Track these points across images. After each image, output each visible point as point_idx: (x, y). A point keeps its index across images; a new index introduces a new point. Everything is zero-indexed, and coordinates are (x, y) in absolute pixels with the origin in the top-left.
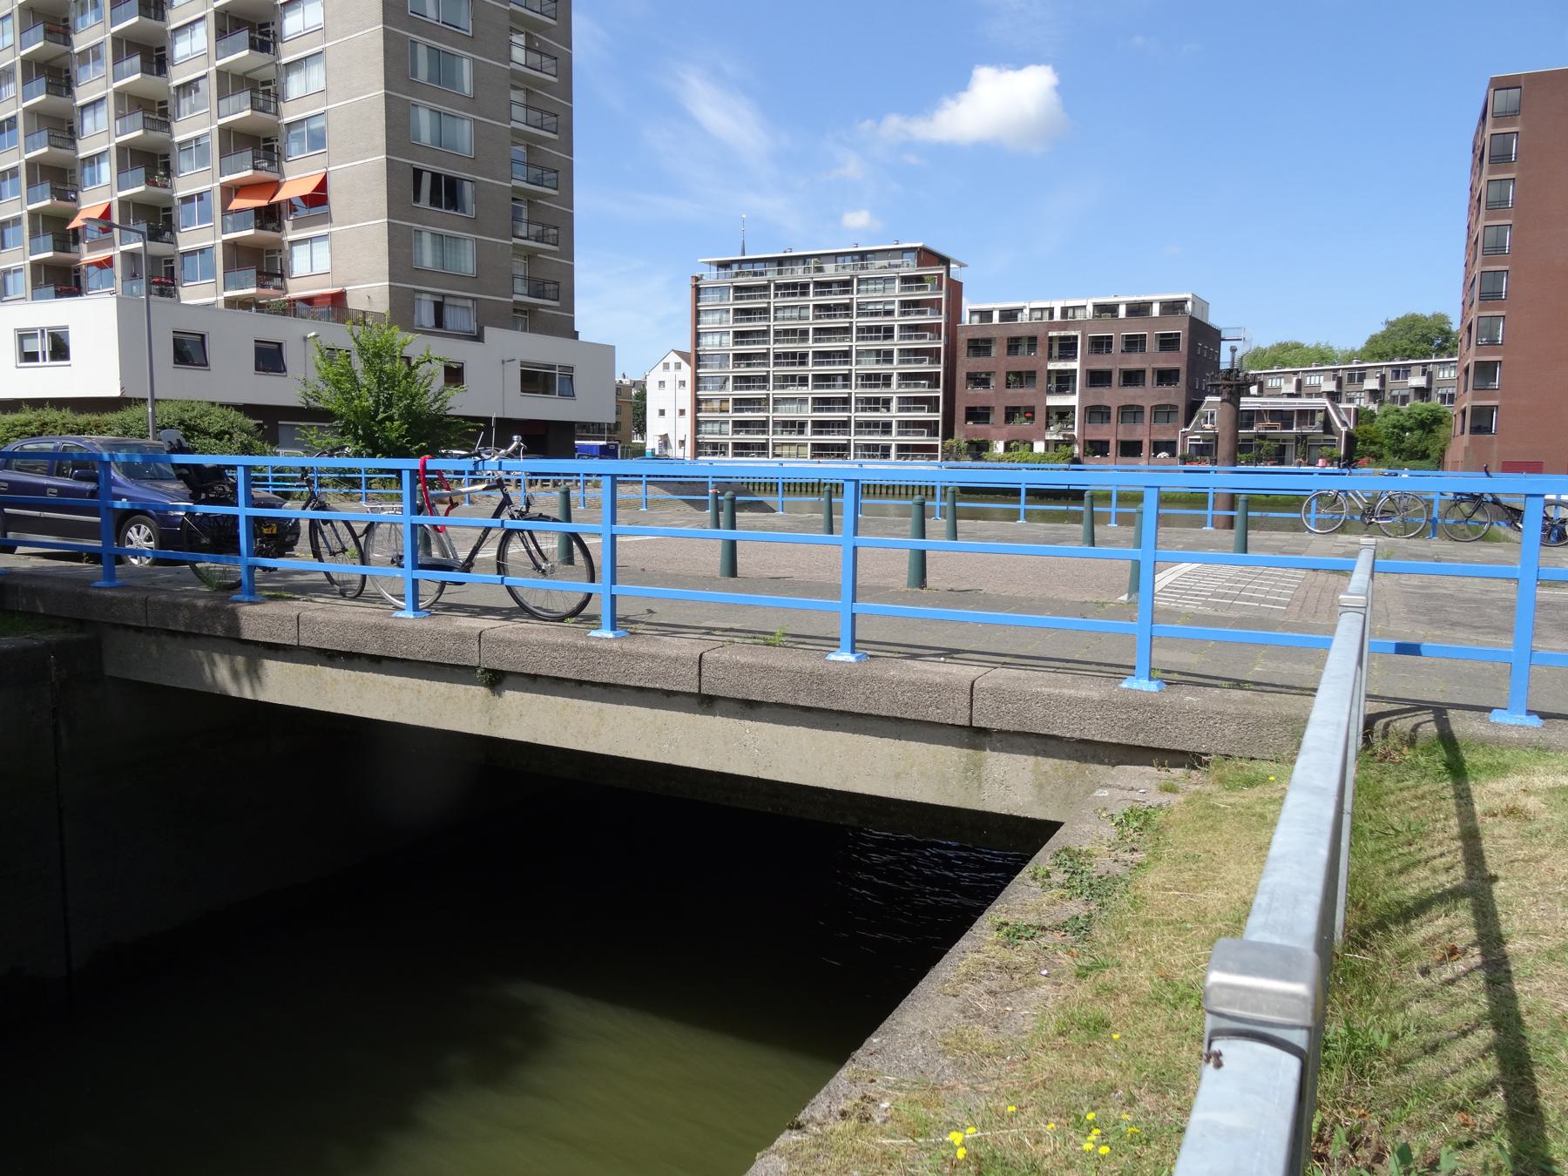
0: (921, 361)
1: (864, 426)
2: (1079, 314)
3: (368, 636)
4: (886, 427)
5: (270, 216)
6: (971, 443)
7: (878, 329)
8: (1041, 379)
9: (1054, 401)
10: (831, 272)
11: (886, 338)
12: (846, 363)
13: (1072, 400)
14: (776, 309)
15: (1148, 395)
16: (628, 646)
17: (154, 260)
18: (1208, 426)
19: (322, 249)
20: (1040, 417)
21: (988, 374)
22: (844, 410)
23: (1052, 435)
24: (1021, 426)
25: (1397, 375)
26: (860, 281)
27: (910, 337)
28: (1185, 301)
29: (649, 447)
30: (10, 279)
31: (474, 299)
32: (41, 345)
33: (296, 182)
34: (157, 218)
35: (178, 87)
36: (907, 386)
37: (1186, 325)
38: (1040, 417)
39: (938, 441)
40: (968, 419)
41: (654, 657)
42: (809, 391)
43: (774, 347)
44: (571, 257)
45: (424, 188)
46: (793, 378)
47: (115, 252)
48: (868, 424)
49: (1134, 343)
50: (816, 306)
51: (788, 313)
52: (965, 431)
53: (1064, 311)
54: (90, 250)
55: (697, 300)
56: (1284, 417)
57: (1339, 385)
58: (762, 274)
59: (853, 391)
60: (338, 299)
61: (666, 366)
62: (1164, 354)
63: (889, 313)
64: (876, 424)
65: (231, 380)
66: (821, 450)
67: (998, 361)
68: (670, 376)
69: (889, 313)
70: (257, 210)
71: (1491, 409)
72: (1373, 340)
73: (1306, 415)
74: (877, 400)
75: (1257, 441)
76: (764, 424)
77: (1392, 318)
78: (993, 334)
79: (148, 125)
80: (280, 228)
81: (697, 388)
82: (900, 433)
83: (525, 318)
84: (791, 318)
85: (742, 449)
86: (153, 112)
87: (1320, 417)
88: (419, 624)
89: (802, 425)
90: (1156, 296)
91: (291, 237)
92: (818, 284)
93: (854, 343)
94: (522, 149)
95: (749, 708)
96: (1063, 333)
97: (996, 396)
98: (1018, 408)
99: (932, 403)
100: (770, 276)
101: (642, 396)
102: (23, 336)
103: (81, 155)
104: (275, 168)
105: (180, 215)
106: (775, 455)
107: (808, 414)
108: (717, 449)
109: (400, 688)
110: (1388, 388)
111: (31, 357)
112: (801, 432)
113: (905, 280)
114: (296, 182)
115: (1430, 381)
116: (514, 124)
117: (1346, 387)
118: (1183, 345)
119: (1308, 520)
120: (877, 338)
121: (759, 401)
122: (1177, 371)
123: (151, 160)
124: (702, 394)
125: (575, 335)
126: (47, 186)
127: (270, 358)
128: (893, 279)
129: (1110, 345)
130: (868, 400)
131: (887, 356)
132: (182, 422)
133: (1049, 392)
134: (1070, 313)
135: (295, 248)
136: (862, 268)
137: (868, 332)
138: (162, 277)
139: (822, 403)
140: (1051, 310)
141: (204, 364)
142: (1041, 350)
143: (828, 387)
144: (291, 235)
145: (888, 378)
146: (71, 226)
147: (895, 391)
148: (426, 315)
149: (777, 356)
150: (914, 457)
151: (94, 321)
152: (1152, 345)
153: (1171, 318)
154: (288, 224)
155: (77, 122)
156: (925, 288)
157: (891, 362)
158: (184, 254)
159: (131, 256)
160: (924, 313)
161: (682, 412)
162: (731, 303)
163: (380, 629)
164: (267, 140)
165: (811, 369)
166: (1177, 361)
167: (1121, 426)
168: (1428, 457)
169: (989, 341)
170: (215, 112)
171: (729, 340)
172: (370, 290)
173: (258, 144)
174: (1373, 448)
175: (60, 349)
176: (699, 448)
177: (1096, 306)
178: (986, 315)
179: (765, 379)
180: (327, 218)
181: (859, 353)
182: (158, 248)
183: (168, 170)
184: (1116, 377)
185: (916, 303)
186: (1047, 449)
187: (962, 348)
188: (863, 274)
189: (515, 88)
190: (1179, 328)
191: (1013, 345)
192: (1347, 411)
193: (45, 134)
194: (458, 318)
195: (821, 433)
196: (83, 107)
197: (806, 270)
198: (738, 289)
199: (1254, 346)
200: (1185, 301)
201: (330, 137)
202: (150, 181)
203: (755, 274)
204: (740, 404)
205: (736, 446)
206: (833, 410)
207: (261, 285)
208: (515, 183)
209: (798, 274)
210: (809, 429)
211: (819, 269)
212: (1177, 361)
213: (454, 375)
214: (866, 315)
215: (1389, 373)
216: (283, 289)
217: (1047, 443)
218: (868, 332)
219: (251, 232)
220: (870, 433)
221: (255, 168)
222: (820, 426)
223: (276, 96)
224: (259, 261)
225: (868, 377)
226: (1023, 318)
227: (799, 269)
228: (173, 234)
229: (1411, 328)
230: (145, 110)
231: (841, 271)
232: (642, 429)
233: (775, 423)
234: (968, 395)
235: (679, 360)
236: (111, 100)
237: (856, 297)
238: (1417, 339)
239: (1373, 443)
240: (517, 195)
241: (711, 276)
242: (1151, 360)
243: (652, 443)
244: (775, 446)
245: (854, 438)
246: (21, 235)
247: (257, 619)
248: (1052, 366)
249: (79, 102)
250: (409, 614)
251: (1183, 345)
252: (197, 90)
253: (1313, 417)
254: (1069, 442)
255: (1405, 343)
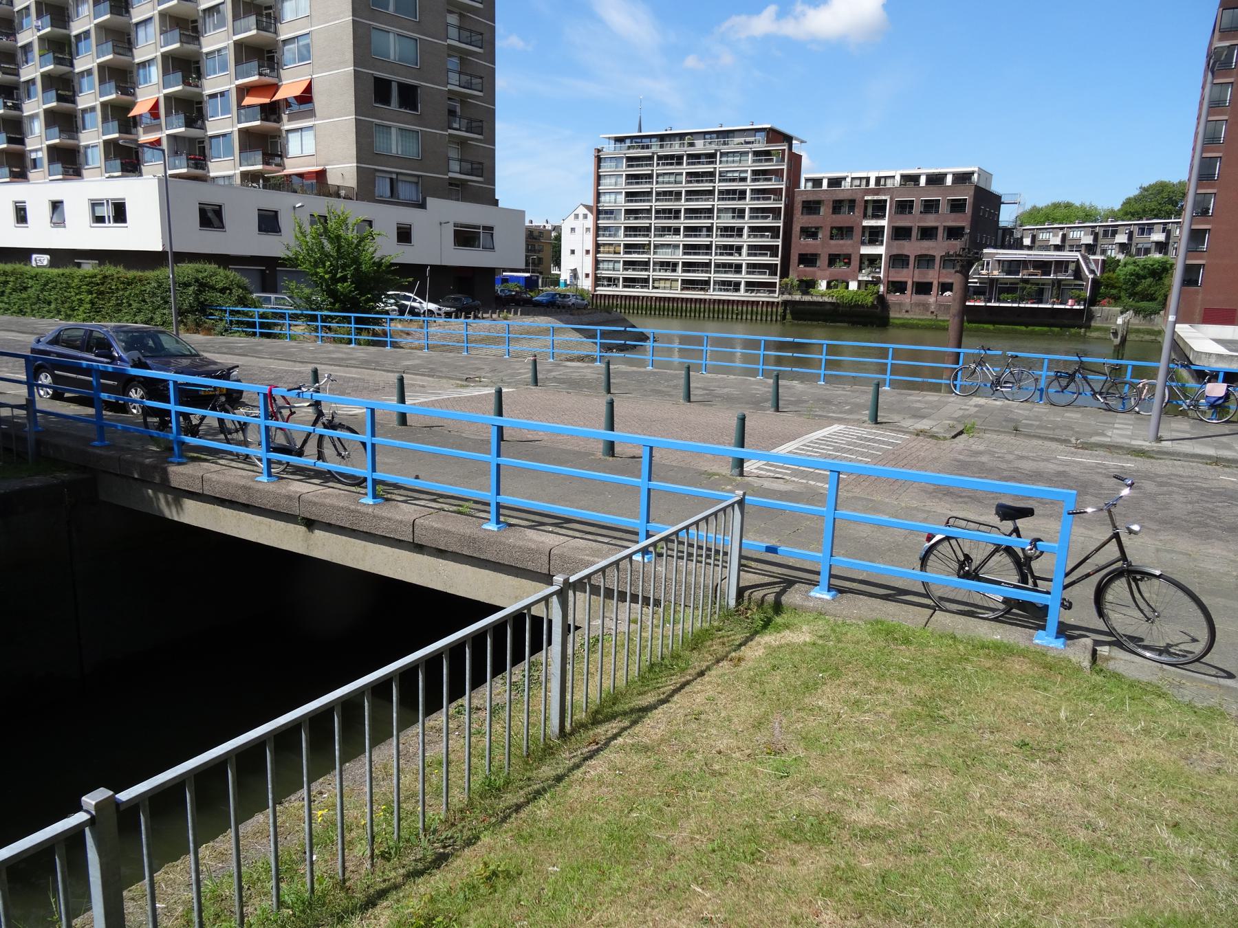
0: (767, 217)
1: (722, 267)
2: (889, 182)
3: (240, 492)
4: (738, 268)
5: (271, 111)
6: (801, 281)
7: (734, 192)
8: (857, 233)
9: (866, 250)
10: (700, 147)
11: (740, 199)
12: (709, 218)
13: (880, 250)
14: (658, 175)
15: (938, 247)
16: (377, 512)
17: (191, 141)
18: (984, 272)
19: (309, 137)
20: (855, 262)
21: (817, 228)
22: (707, 254)
23: (864, 277)
24: (840, 269)
25: (1142, 231)
26: (722, 154)
27: (758, 199)
28: (973, 173)
29: (562, 279)
30: (89, 151)
31: (418, 176)
32: (107, 211)
33: (290, 87)
34: (191, 109)
35: (204, 11)
36: (755, 236)
37: (972, 193)
38: (855, 262)
39: (777, 280)
40: (800, 263)
41: (390, 519)
42: (680, 239)
43: (655, 205)
44: (493, 143)
45: (379, 92)
46: (669, 229)
47: (163, 135)
48: (724, 265)
49: (930, 206)
50: (688, 174)
51: (666, 179)
52: (797, 272)
53: (878, 179)
54: (145, 132)
55: (599, 167)
56: (1044, 266)
57: (1096, 239)
58: (648, 147)
59: (714, 239)
60: (321, 175)
61: (577, 216)
62: (953, 215)
63: (744, 180)
64: (730, 265)
65: (241, 238)
66: (688, 284)
67: (825, 217)
68: (580, 224)
69: (744, 179)
70: (262, 106)
71: (1199, 266)
72: (1128, 202)
73: (1061, 265)
74: (731, 247)
75: (1021, 285)
76: (647, 263)
77: (1146, 185)
78: (823, 197)
79: (184, 39)
80: (279, 120)
81: (597, 235)
82: (748, 273)
83: (458, 190)
84: (669, 183)
85: (629, 282)
86: (187, 30)
87: (1072, 267)
88: (273, 487)
89: (675, 265)
90: (950, 169)
91: (287, 127)
92: (689, 156)
93: (716, 203)
94: (456, 60)
95: (440, 553)
96: (876, 198)
97: (822, 245)
98: (839, 255)
99: (773, 250)
100: (654, 149)
101: (558, 238)
102: (95, 204)
103: (137, 61)
104: (275, 74)
105: (208, 108)
106: (654, 287)
107: (679, 256)
108: (612, 281)
109: (261, 523)
110: (1135, 241)
111: (100, 220)
112: (674, 271)
113: (756, 153)
114: (290, 87)
115: (1168, 237)
116: (449, 42)
117: (1101, 241)
118: (968, 209)
119: (955, 386)
120: (733, 199)
121: (643, 246)
122: (963, 228)
123: (186, 66)
124: (601, 239)
125: (496, 203)
126: (113, 84)
127: (269, 222)
128: (747, 153)
129: (911, 207)
130: (725, 247)
131: (740, 213)
132: (197, 280)
133: (863, 243)
134: (882, 182)
135: (291, 136)
136: (725, 144)
137: (726, 194)
138: (196, 152)
139: (689, 249)
140: (868, 179)
141: (221, 226)
142: (858, 211)
143: (696, 236)
144: (287, 126)
145: (741, 230)
146: (131, 114)
147: (746, 240)
148: (383, 188)
149: (657, 212)
150: (758, 291)
151: (142, 193)
152: (944, 208)
153: (961, 187)
154: (285, 117)
155: (133, 34)
156: (771, 160)
157: (743, 217)
158: (211, 137)
159: (173, 138)
160: (770, 180)
161: (588, 252)
162: (624, 169)
163: (246, 488)
164: (270, 52)
165: (683, 222)
166: (962, 221)
167: (917, 271)
168: (1155, 299)
169: (819, 203)
170: (231, 31)
171: (622, 198)
172: (343, 172)
173: (262, 55)
174: (1114, 291)
175: (120, 212)
176: (597, 281)
177: (903, 176)
178: (817, 182)
179: (648, 229)
180: (311, 114)
181: (719, 210)
182: (194, 132)
183: (200, 76)
184: (914, 233)
185: (764, 172)
186: (859, 287)
187: (798, 207)
188: (725, 149)
189: (450, 12)
190: (967, 195)
191: (837, 206)
192: (1096, 261)
193: (110, 44)
194: (405, 191)
195: (689, 271)
196: (137, 24)
197: (682, 145)
198: (629, 159)
199: (1028, 207)
200: (973, 173)
201: (314, 51)
202: (185, 82)
203: (643, 147)
204: (629, 248)
205: (625, 280)
206: (698, 254)
207: (266, 163)
208: (450, 87)
209: (676, 149)
210: (680, 268)
211: (692, 145)
212: (962, 221)
213: (404, 235)
214: (725, 181)
215: (1136, 230)
216: (281, 166)
217: (860, 282)
218: (726, 194)
219: (258, 123)
220: (726, 272)
221: (260, 74)
222: (688, 266)
223: (275, 19)
224: (264, 143)
225: (726, 229)
226: (846, 185)
227: (676, 143)
228: (203, 122)
229: (1160, 192)
230: (181, 28)
231: (708, 146)
232: (558, 263)
233: (655, 263)
234: (802, 244)
235: (586, 211)
236: (157, 20)
237: (719, 167)
238: (1158, 202)
239: (1114, 287)
240: (452, 95)
241: (609, 149)
242: (943, 219)
243: (565, 275)
244: (654, 280)
245: (713, 276)
246: (96, 119)
247: (181, 474)
248: (866, 223)
249: (135, 20)
250: (264, 479)
251: (968, 209)
252: (218, 12)
253: (1067, 267)
254: (876, 282)
255: (1153, 205)
